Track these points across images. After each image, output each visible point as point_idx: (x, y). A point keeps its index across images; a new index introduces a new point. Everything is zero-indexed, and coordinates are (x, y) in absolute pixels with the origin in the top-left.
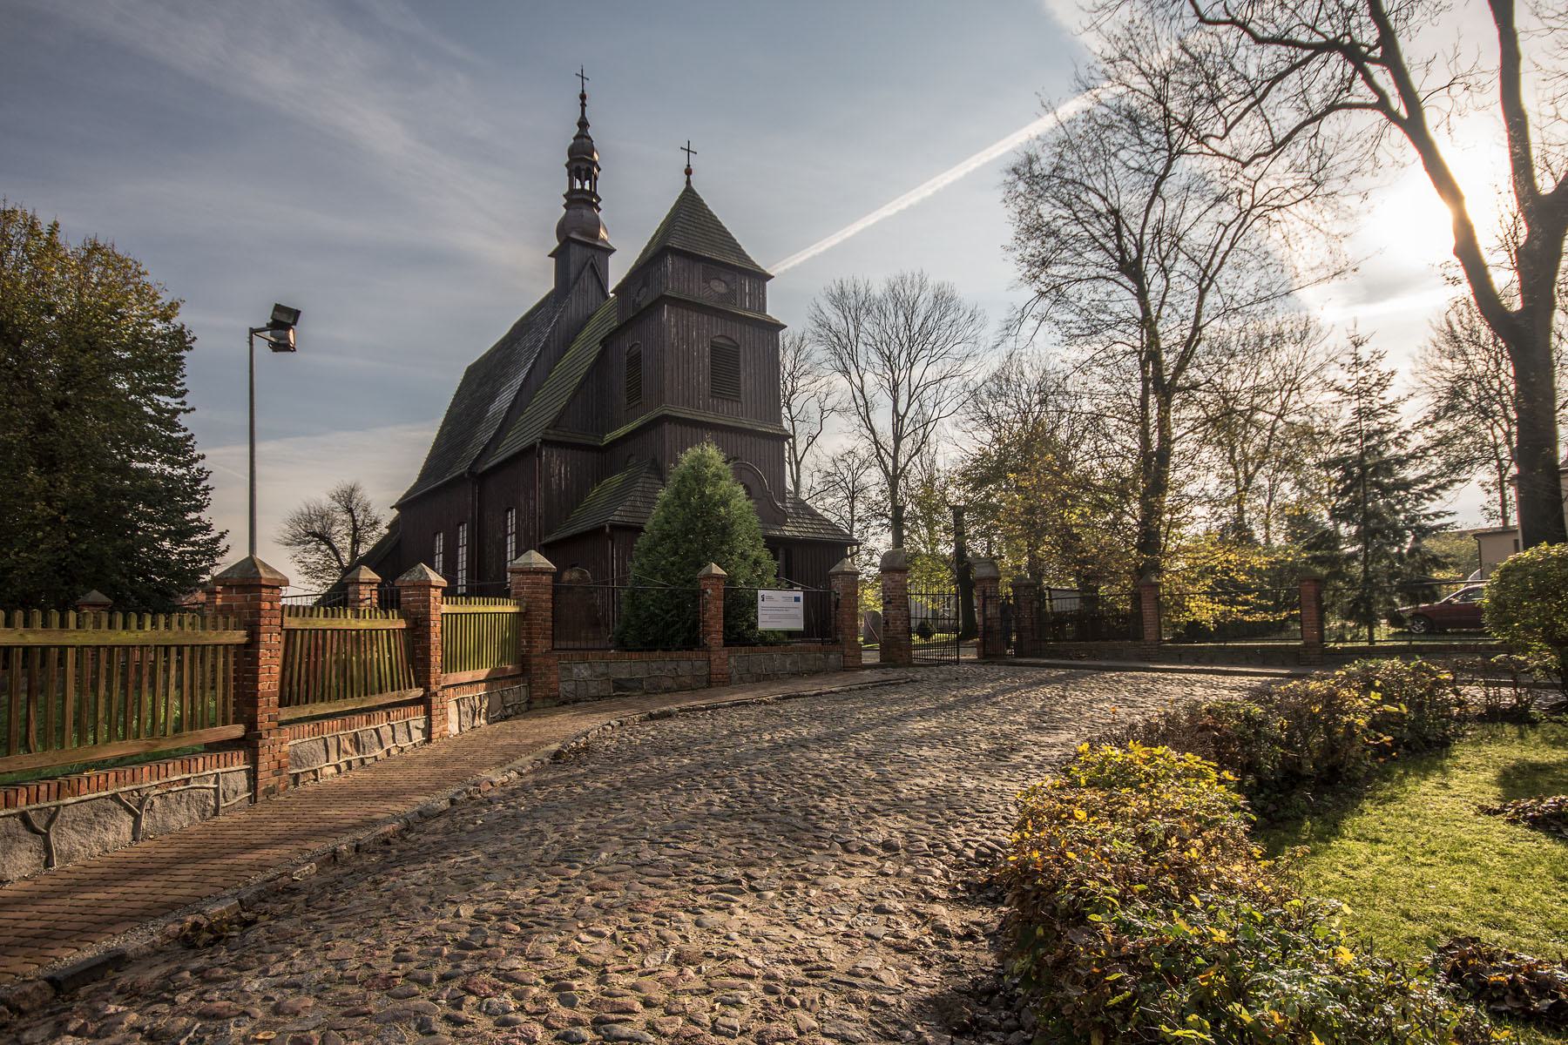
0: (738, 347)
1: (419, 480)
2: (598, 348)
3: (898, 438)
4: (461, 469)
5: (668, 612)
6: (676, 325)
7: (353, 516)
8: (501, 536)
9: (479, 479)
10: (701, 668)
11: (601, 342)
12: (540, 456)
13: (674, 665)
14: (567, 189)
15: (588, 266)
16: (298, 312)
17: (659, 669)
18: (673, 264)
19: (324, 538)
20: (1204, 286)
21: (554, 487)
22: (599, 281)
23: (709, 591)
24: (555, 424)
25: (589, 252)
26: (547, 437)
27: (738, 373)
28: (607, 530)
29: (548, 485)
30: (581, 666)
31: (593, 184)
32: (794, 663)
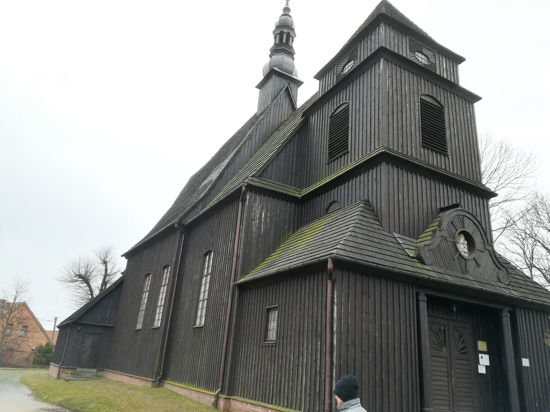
7: (106, 267)
8: (197, 277)
12: (244, 201)
15: (284, 89)
19: (85, 279)
21: (254, 229)
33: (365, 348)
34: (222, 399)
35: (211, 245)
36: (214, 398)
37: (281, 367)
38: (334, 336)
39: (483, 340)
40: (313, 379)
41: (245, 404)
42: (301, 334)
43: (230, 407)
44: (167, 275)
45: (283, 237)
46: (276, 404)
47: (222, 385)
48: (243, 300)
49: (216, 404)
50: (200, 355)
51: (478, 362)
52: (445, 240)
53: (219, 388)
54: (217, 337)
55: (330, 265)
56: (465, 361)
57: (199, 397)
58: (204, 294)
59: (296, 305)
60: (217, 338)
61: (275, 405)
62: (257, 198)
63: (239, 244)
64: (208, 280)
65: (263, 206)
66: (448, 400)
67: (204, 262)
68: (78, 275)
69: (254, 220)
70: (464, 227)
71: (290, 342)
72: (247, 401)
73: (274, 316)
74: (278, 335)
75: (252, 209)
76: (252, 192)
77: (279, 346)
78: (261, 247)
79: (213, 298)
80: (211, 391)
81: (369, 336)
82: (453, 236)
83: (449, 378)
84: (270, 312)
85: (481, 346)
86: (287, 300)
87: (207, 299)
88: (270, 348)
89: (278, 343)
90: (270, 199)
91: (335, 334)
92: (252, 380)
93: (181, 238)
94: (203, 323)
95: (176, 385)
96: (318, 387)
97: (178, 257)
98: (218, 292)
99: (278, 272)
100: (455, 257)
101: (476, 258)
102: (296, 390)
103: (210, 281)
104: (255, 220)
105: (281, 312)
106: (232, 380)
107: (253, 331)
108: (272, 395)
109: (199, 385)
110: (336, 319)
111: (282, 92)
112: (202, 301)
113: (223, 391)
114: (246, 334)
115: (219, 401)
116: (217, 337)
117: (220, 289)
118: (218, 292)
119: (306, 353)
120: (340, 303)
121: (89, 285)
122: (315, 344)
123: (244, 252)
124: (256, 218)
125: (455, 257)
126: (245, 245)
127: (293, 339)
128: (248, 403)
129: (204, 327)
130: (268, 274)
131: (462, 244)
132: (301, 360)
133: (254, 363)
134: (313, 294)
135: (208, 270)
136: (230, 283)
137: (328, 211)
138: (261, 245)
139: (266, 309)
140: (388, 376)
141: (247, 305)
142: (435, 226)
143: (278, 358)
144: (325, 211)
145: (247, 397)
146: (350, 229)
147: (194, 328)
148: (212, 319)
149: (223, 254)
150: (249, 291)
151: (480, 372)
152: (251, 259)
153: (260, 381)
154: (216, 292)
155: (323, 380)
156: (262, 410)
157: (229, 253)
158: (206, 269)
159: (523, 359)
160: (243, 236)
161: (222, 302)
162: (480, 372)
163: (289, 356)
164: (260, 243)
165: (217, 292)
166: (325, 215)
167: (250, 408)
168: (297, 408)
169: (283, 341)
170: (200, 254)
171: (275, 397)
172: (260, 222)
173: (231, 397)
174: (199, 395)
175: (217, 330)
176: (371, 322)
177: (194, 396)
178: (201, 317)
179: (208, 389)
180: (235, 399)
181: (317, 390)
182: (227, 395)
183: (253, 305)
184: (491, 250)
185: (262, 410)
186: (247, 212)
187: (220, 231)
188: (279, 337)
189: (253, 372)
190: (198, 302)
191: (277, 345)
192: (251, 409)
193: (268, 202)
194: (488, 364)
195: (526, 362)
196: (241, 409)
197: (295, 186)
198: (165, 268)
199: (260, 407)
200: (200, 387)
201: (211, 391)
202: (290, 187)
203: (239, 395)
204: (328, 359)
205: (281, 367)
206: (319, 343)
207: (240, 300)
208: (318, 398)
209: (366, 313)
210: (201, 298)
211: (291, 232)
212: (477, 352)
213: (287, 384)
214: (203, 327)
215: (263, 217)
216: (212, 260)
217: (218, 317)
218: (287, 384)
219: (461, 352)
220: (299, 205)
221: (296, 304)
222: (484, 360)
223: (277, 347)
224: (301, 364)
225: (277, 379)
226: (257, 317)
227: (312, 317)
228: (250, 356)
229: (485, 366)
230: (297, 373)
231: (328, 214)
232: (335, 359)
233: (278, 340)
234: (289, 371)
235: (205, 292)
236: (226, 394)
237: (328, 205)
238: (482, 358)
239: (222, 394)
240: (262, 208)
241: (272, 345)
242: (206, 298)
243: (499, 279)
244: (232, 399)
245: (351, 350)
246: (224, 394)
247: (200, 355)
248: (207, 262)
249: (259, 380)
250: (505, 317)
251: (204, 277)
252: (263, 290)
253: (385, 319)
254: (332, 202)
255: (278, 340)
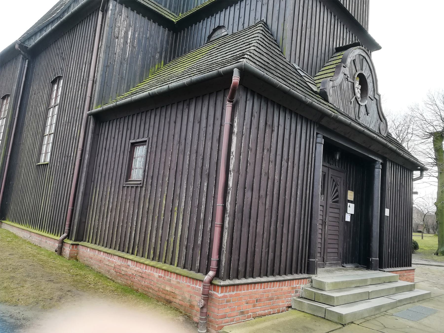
8: (43, 108)
12: (105, 11)
21: (118, 50)
29: (110, 46)
33: (263, 193)
34: (68, 245)
35: (61, 70)
36: (58, 243)
37: (148, 212)
38: (230, 175)
39: (352, 190)
40: (193, 228)
41: (97, 251)
42: (179, 173)
43: (78, 254)
45: (152, 66)
46: (138, 254)
47: (69, 230)
48: (100, 134)
49: (60, 251)
50: (44, 195)
51: (346, 211)
52: (347, 80)
53: (65, 232)
54: (65, 175)
55: (236, 78)
56: (336, 209)
57: (41, 241)
58: (50, 128)
59: (173, 138)
60: (64, 177)
61: (137, 255)
62: (123, 11)
63: (97, 66)
64: (56, 112)
65: (130, 23)
66: (320, 248)
67: (51, 91)
69: (118, 38)
70: (362, 70)
71: (162, 183)
72: (100, 249)
73: (140, 151)
74: (146, 174)
75: (116, 23)
76: (116, 1)
77: (146, 188)
78: (125, 74)
79: (61, 132)
80: (55, 235)
81: (268, 178)
82: (353, 77)
83: (323, 226)
84: (136, 148)
85: (349, 195)
86: (161, 133)
87: (54, 134)
88: (134, 190)
89: (145, 183)
90: (139, 17)
91: (232, 172)
92: (108, 226)
93: (24, 64)
94: (48, 160)
95: (15, 226)
96: (200, 239)
97: (19, 86)
98: (68, 124)
99: (151, 94)
100: (352, 101)
101: (367, 106)
102: (168, 240)
103: (57, 113)
104: (119, 38)
105: (151, 147)
106: (82, 223)
107: (111, 169)
108: (134, 244)
109: (41, 228)
110: (234, 153)
112: (48, 135)
113: (70, 237)
114: (102, 173)
115: (65, 247)
116: (65, 175)
117: (70, 121)
118: (68, 124)
119: (185, 197)
120: (241, 134)
122: (199, 186)
123: (103, 76)
124: (120, 36)
125: (352, 101)
126: (106, 66)
127: (166, 180)
128: (101, 251)
129: (49, 164)
130: (137, 98)
131: (357, 88)
132: (177, 205)
133: (111, 207)
134: (200, 122)
135: (56, 100)
136: (83, 113)
137: (210, 38)
138: (125, 72)
139: (130, 144)
140: (282, 225)
141: (105, 140)
142: (333, 64)
143: (144, 202)
144: (206, 39)
145: (100, 244)
146: (253, 45)
147: (37, 165)
148: (59, 156)
149: (75, 79)
150: (108, 123)
151: (346, 220)
152: (112, 86)
153: (118, 227)
154: (65, 125)
155: (208, 229)
156: (119, 261)
157: (83, 77)
158: (54, 99)
159: (386, 209)
160: (102, 55)
161: (73, 136)
162: (346, 220)
163: (160, 199)
164: (125, 68)
165: (67, 124)
166: (206, 44)
167: (104, 257)
168: (167, 261)
169: (152, 181)
170: (47, 82)
171: (137, 246)
172: (126, 42)
173: (80, 243)
174: (41, 239)
175: (65, 168)
176: (272, 162)
177: (35, 239)
178: (46, 153)
179: (52, 232)
180: (84, 246)
181: (199, 242)
182: (75, 240)
183: (112, 140)
184: (378, 99)
185: (119, 261)
186: (109, 25)
187: (73, 52)
188: (147, 176)
189: (109, 216)
190: (43, 136)
191: (144, 185)
192: (105, 258)
193: (136, 19)
194: (353, 213)
195: (387, 212)
196: (93, 257)
197: (170, 9)
199: (116, 257)
200: (43, 230)
201: (55, 235)
202: (164, 9)
203: (90, 241)
204: (219, 204)
205: (148, 212)
206: (206, 184)
207: (96, 134)
208: (200, 252)
209: (268, 150)
210: (47, 132)
211: (163, 63)
212: (347, 201)
213: (154, 233)
214: (48, 164)
215: (129, 37)
216: (61, 88)
217: (67, 153)
218: (154, 233)
219: (333, 201)
220: (173, 33)
221: (174, 136)
223: (144, 189)
224: (176, 209)
225: (141, 226)
226: (118, 153)
227: (197, 152)
228: (106, 198)
229: (350, 215)
230: (170, 220)
231: (211, 42)
232: (229, 205)
233: (145, 180)
234: (158, 217)
235: (51, 124)
236: (73, 239)
237: (211, 31)
238: (349, 207)
239: (68, 239)
241: (136, 185)
242: (53, 132)
243: (379, 131)
244: (81, 245)
245: (248, 194)
246: (71, 240)
247: (44, 195)
248: (55, 91)
249: (117, 225)
250: (377, 168)
251: (51, 108)
252: (126, 121)
253: (286, 159)
254: (216, 28)
255: (145, 180)
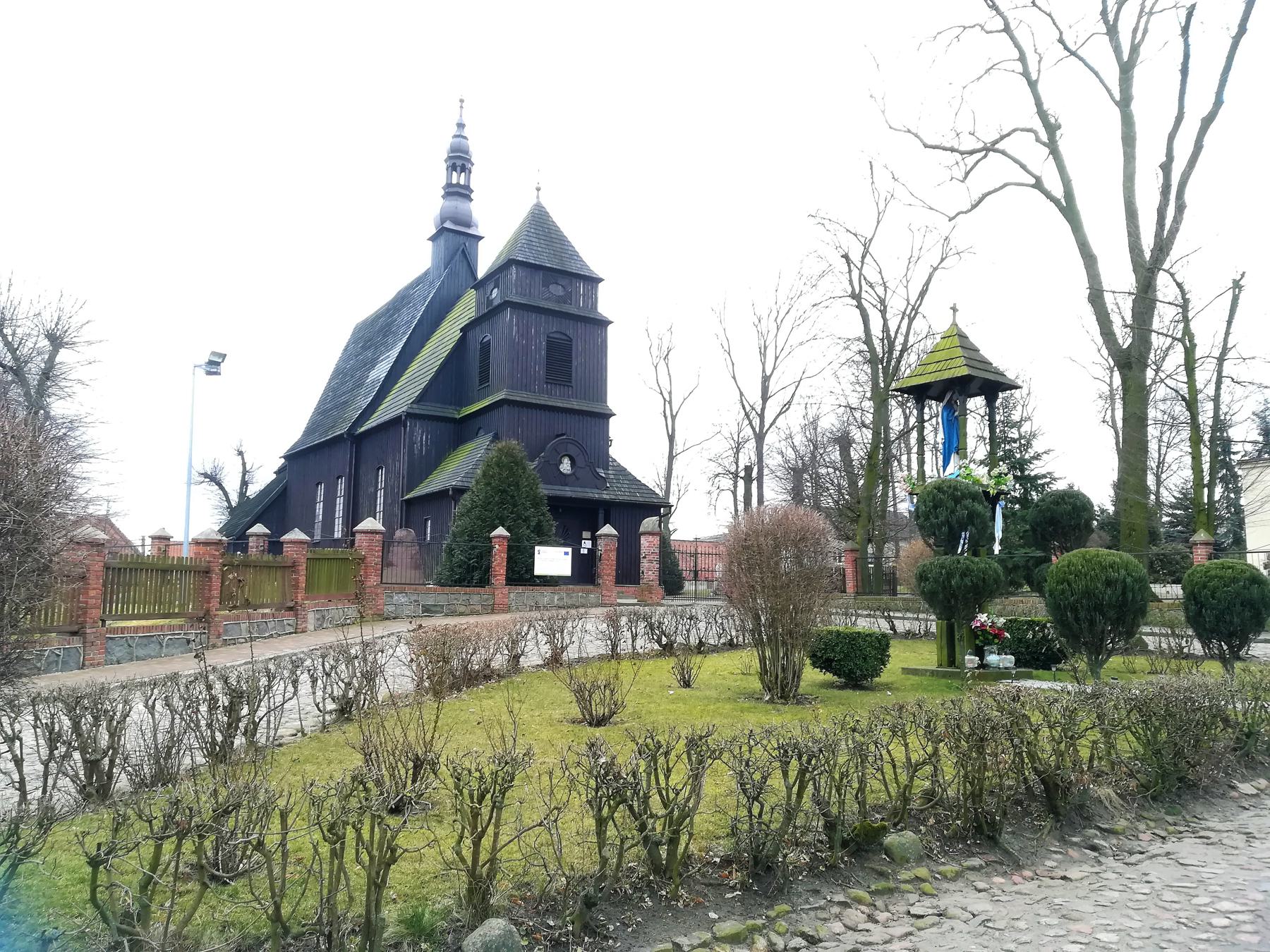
0: (571, 340)
1: (303, 436)
2: (458, 335)
3: (765, 397)
4: (341, 430)
5: (470, 560)
6: (517, 325)
8: (372, 490)
9: (357, 441)
10: (487, 600)
11: (462, 330)
12: (405, 427)
13: (467, 597)
14: (444, 183)
15: (460, 252)
16: (226, 355)
17: (456, 599)
18: (517, 273)
19: (213, 478)
20: (914, 312)
21: (416, 452)
22: (469, 265)
23: (497, 546)
24: (420, 399)
25: (462, 239)
26: (411, 411)
27: (571, 362)
28: (450, 493)
30: (400, 595)
31: (468, 179)
32: (561, 599)
44: (341, 486)
68: (202, 474)
111: (457, 256)
121: (222, 488)
198: (338, 478)
222: (587, 544)
240: (423, 432)
